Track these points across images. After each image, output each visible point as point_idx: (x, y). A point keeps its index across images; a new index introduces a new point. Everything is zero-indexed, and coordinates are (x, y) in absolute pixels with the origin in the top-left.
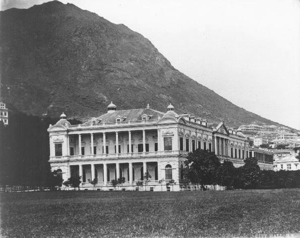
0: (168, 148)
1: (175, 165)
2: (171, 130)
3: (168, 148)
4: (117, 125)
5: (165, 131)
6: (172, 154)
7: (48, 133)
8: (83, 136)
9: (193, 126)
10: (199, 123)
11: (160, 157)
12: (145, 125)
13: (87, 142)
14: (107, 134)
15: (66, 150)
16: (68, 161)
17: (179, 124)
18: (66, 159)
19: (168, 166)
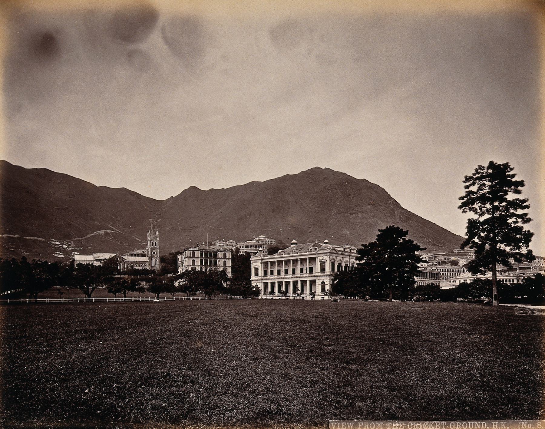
0: (323, 270)
1: (328, 282)
2: (325, 257)
3: (323, 270)
4: (291, 255)
5: (321, 258)
6: (325, 274)
7: (251, 261)
8: (293, 260)
9: (342, 253)
10: (348, 250)
11: (318, 276)
12: (308, 255)
13: (314, 263)
14: (310, 259)
15: (261, 272)
16: (262, 279)
17: (330, 253)
18: (261, 278)
19: (323, 282)
